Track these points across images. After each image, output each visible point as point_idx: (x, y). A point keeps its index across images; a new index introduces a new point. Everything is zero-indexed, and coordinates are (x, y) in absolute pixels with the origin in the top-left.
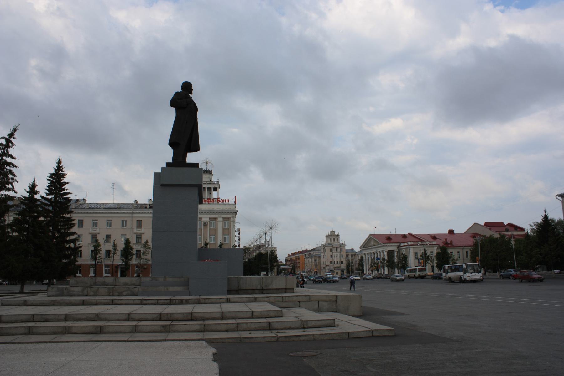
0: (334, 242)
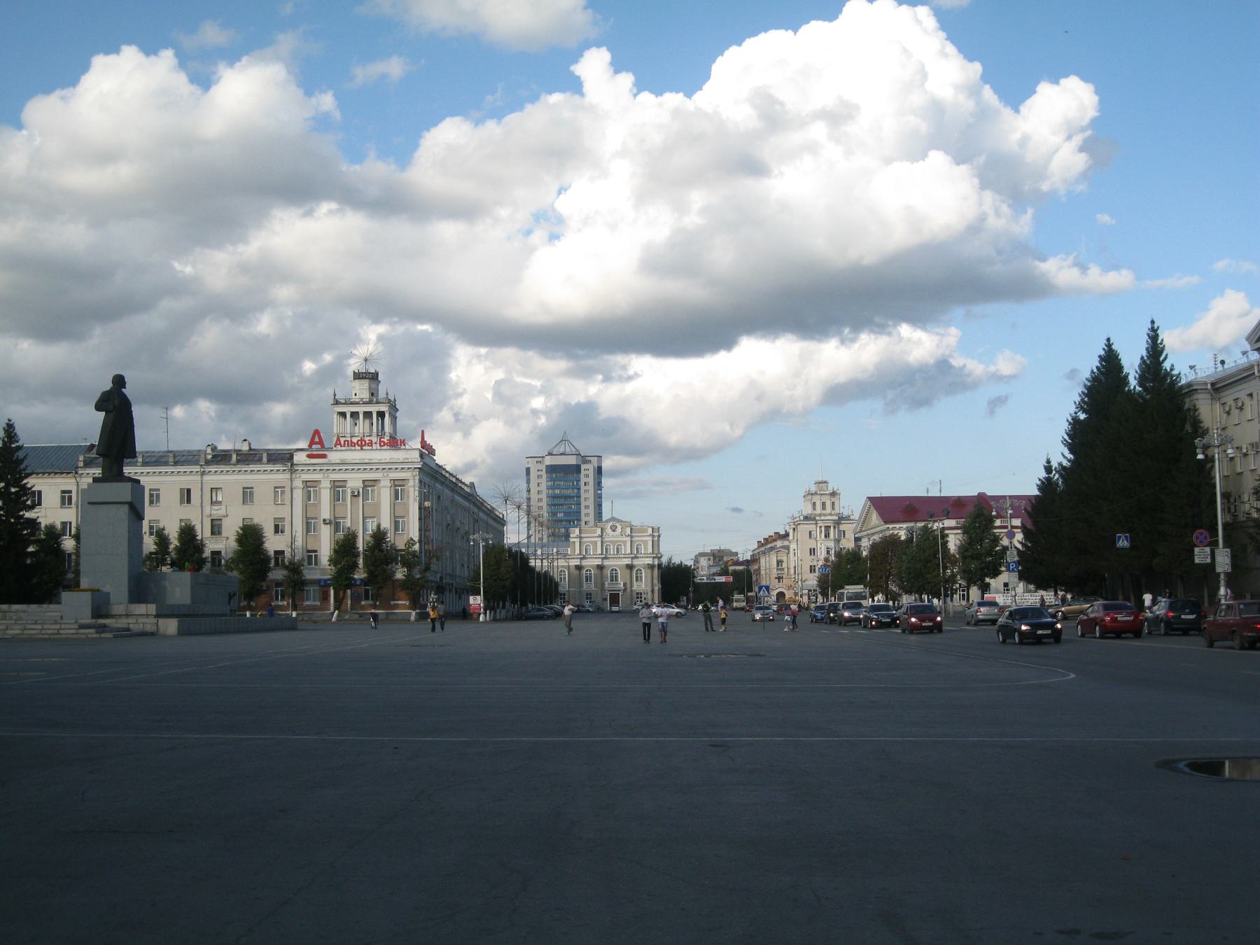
0: (824, 512)
